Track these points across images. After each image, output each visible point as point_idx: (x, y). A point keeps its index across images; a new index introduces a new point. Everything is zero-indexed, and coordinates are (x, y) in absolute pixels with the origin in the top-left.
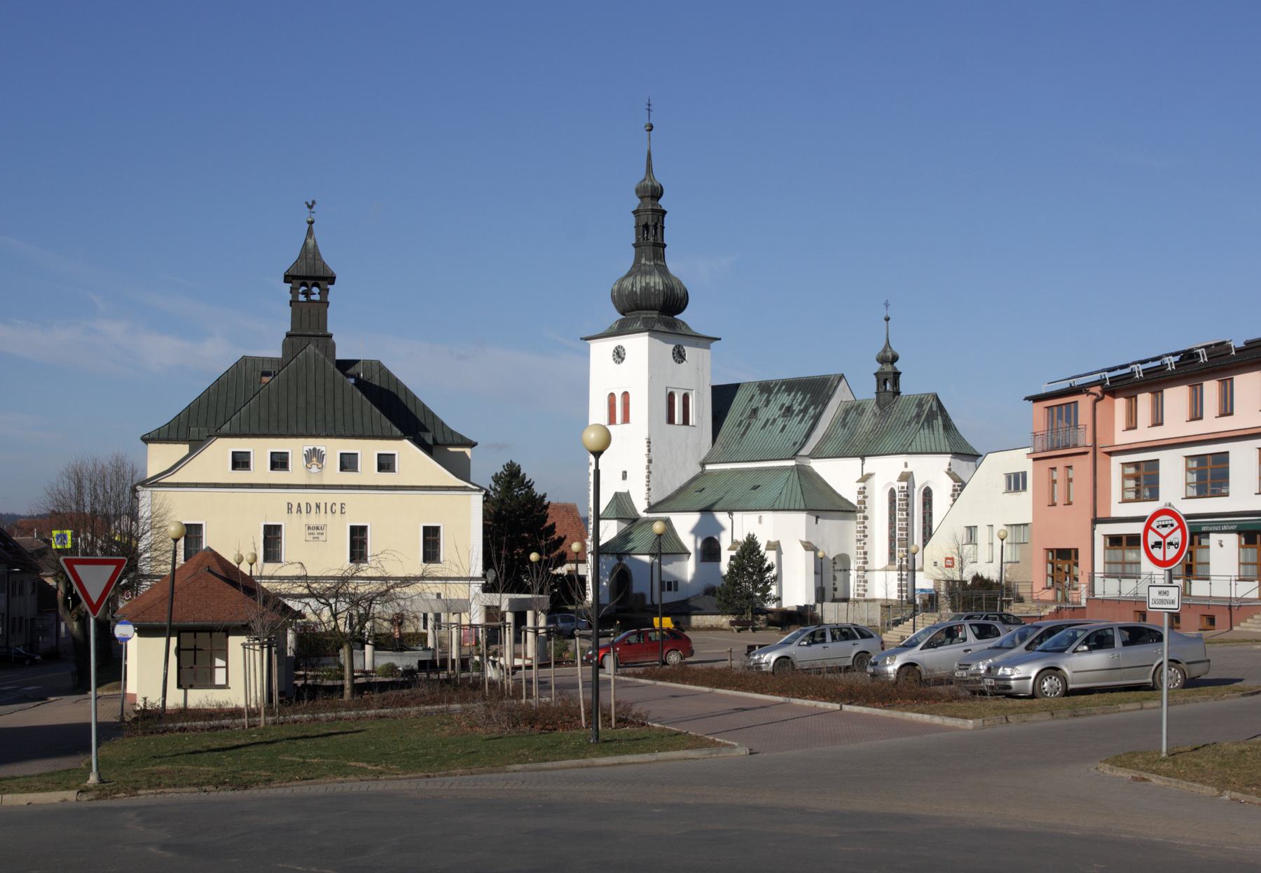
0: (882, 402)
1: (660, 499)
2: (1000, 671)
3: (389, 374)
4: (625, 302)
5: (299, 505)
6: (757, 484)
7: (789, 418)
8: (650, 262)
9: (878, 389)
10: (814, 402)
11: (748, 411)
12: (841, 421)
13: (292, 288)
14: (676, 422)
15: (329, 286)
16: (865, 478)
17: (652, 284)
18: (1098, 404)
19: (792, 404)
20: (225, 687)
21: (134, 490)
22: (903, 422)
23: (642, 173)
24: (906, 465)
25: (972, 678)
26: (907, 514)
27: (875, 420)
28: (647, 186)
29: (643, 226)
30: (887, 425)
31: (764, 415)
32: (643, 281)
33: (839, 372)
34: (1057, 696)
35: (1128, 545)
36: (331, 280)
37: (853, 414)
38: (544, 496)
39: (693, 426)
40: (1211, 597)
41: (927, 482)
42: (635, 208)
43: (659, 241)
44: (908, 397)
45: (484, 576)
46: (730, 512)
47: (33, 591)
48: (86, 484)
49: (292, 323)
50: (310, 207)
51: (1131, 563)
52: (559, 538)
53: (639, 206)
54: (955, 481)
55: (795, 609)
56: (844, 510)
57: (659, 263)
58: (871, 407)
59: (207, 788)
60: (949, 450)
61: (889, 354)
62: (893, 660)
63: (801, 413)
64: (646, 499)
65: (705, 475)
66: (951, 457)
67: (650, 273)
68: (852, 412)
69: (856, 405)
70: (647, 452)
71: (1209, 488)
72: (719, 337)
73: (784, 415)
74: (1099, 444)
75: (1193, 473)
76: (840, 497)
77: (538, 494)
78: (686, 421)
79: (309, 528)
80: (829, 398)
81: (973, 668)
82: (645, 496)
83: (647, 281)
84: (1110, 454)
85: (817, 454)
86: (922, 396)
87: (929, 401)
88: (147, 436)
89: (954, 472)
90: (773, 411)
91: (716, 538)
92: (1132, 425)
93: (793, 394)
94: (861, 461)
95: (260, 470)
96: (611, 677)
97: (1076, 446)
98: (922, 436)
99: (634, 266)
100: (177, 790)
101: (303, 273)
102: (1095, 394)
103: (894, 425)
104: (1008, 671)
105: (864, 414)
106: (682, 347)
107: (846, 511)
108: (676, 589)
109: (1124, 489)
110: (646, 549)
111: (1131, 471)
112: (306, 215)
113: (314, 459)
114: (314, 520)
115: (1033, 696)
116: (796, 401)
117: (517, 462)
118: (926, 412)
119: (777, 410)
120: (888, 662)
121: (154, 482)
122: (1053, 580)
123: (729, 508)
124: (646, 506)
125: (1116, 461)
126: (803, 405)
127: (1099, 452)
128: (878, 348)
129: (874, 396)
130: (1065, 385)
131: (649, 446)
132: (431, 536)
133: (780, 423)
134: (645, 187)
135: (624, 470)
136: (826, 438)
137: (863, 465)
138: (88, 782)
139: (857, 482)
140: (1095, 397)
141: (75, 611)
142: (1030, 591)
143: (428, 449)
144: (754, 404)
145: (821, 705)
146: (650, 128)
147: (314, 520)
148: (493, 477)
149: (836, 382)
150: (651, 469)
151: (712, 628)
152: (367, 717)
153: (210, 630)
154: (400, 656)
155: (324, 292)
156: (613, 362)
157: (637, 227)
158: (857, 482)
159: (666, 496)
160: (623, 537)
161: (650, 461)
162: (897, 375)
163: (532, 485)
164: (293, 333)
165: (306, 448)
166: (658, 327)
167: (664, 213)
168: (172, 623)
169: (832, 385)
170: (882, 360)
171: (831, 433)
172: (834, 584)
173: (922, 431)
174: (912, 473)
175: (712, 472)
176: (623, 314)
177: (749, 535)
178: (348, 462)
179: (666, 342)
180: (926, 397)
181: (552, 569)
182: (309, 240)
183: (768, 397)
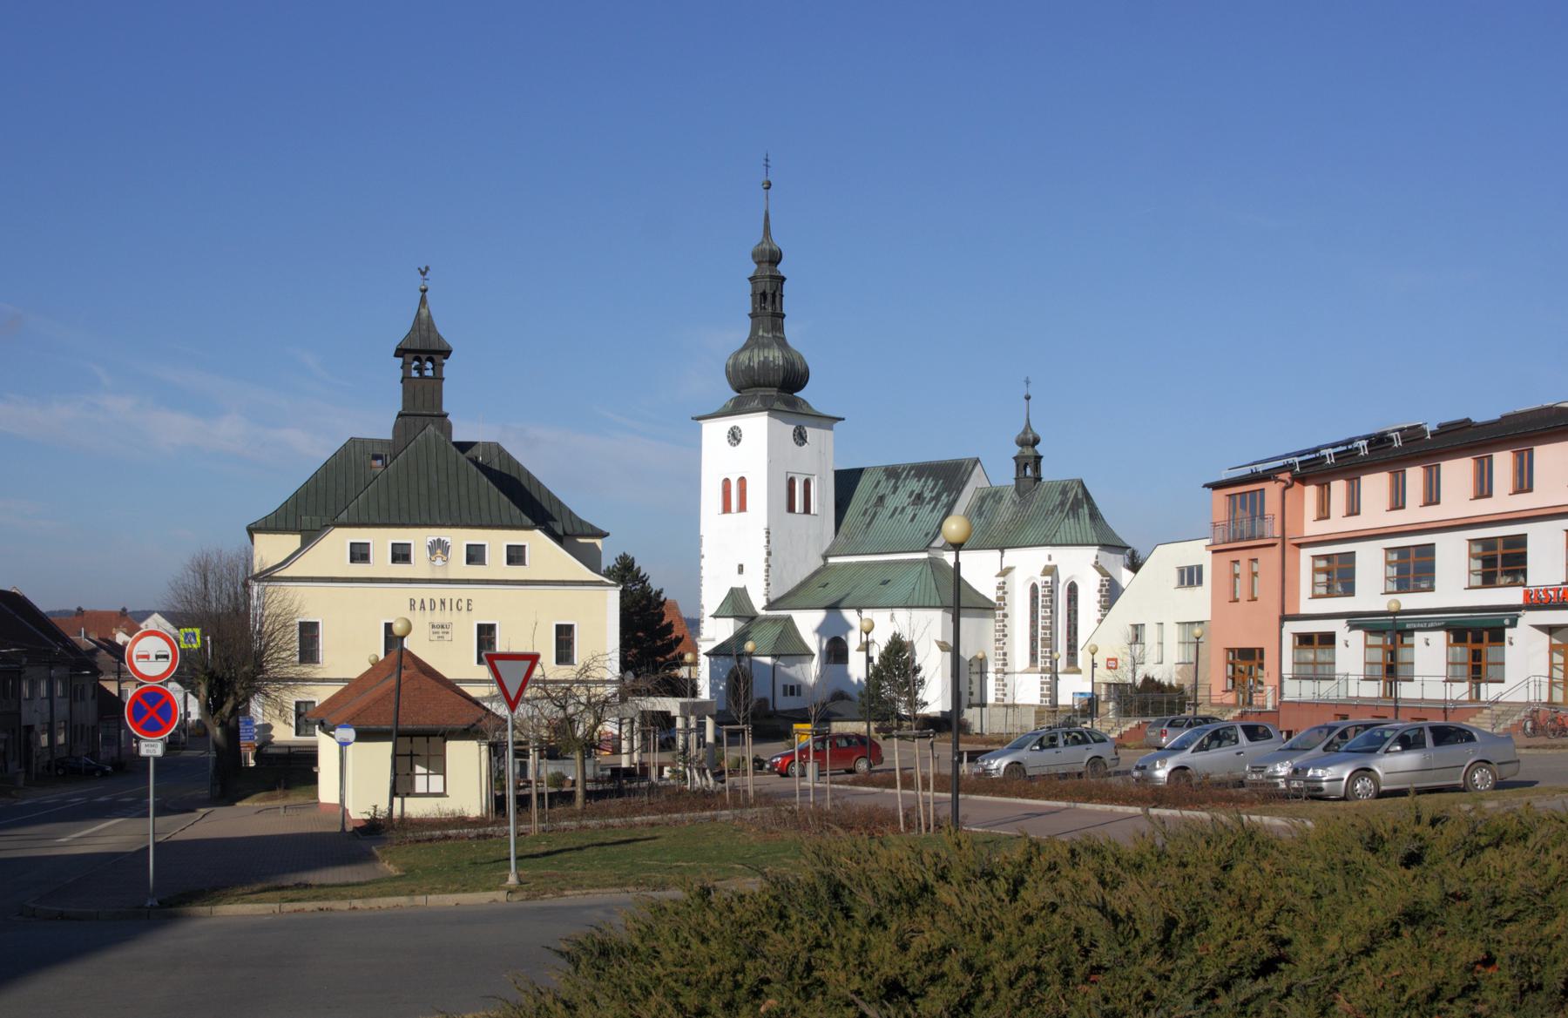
0: (1022, 488)
1: (780, 595)
2: (1310, 773)
3: (509, 457)
5: (422, 601)
6: (887, 578)
9: (1017, 474)
11: (874, 499)
13: (404, 363)
14: (797, 510)
15: (444, 361)
16: (1005, 572)
17: (771, 359)
18: (1287, 492)
19: (922, 492)
20: (443, 795)
21: (246, 585)
23: (758, 236)
24: (1050, 558)
25: (1269, 781)
26: (1051, 612)
31: (892, 502)
32: (761, 354)
33: (972, 455)
34: (1488, 789)
35: (1320, 644)
36: (446, 353)
37: (989, 503)
38: (661, 592)
40: (1423, 699)
41: (1072, 577)
42: (751, 275)
43: (778, 311)
45: (622, 679)
46: (859, 610)
47: (93, 697)
48: (211, 577)
49: (404, 401)
50: (423, 273)
51: (1324, 663)
52: (677, 637)
53: (756, 272)
54: (1103, 575)
55: (939, 715)
56: (985, 608)
57: (778, 334)
58: (1010, 495)
59: (629, 889)
60: (1096, 541)
61: (1030, 436)
62: (1163, 764)
67: (768, 346)
70: (765, 544)
71: (1412, 582)
73: (914, 503)
74: (1288, 534)
75: (1393, 567)
76: (976, 592)
78: (807, 510)
79: (433, 626)
80: (964, 484)
81: (1270, 770)
84: (1299, 546)
88: (253, 526)
90: (901, 498)
91: (843, 637)
92: (1324, 514)
93: (923, 480)
94: (1000, 553)
95: (381, 563)
96: (811, 785)
97: (1262, 537)
98: (1067, 526)
99: (750, 338)
100: (601, 891)
101: (417, 346)
102: (1283, 481)
104: (1320, 772)
108: (799, 694)
109: (1314, 584)
110: (768, 651)
111: (1322, 564)
112: (418, 282)
113: (439, 551)
114: (439, 617)
115: (1345, 799)
116: (928, 487)
117: (631, 554)
120: (1158, 766)
121: (267, 576)
122: (1234, 682)
123: (857, 605)
124: (764, 603)
125: (1306, 554)
127: (1289, 544)
128: (1018, 430)
129: (1013, 482)
130: (1246, 471)
131: (768, 537)
132: (564, 635)
134: (763, 251)
138: (509, 883)
140: (1284, 485)
141: (217, 715)
142: (1207, 693)
143: (558, 539)
144: (881, 491)
145: (1120, 809)
146: (768, 186)
147: (439, 617)
150: (770, 562)
152: (636, 825)
153: (428, 734)
154: (563, 764)
155: (438, 368)
156: (728, 445)
157: (754, 294)
159: (786, 591)
160: (741, 637)
161: (769, 554)
162: (1038, 458)
164: (406, 412)
165: (430, 539)
166: (778, 405)
167: (783, 279)
168: (400, 727)
169: (966, 469)
170: (1022, 443)
173: (1066, 520)
175: (835, 565)
176: (739, 392)
177: (895, 634)
178: (475, 555)
179: (787, 423)
182: (422, 310)
183: (896, 483)
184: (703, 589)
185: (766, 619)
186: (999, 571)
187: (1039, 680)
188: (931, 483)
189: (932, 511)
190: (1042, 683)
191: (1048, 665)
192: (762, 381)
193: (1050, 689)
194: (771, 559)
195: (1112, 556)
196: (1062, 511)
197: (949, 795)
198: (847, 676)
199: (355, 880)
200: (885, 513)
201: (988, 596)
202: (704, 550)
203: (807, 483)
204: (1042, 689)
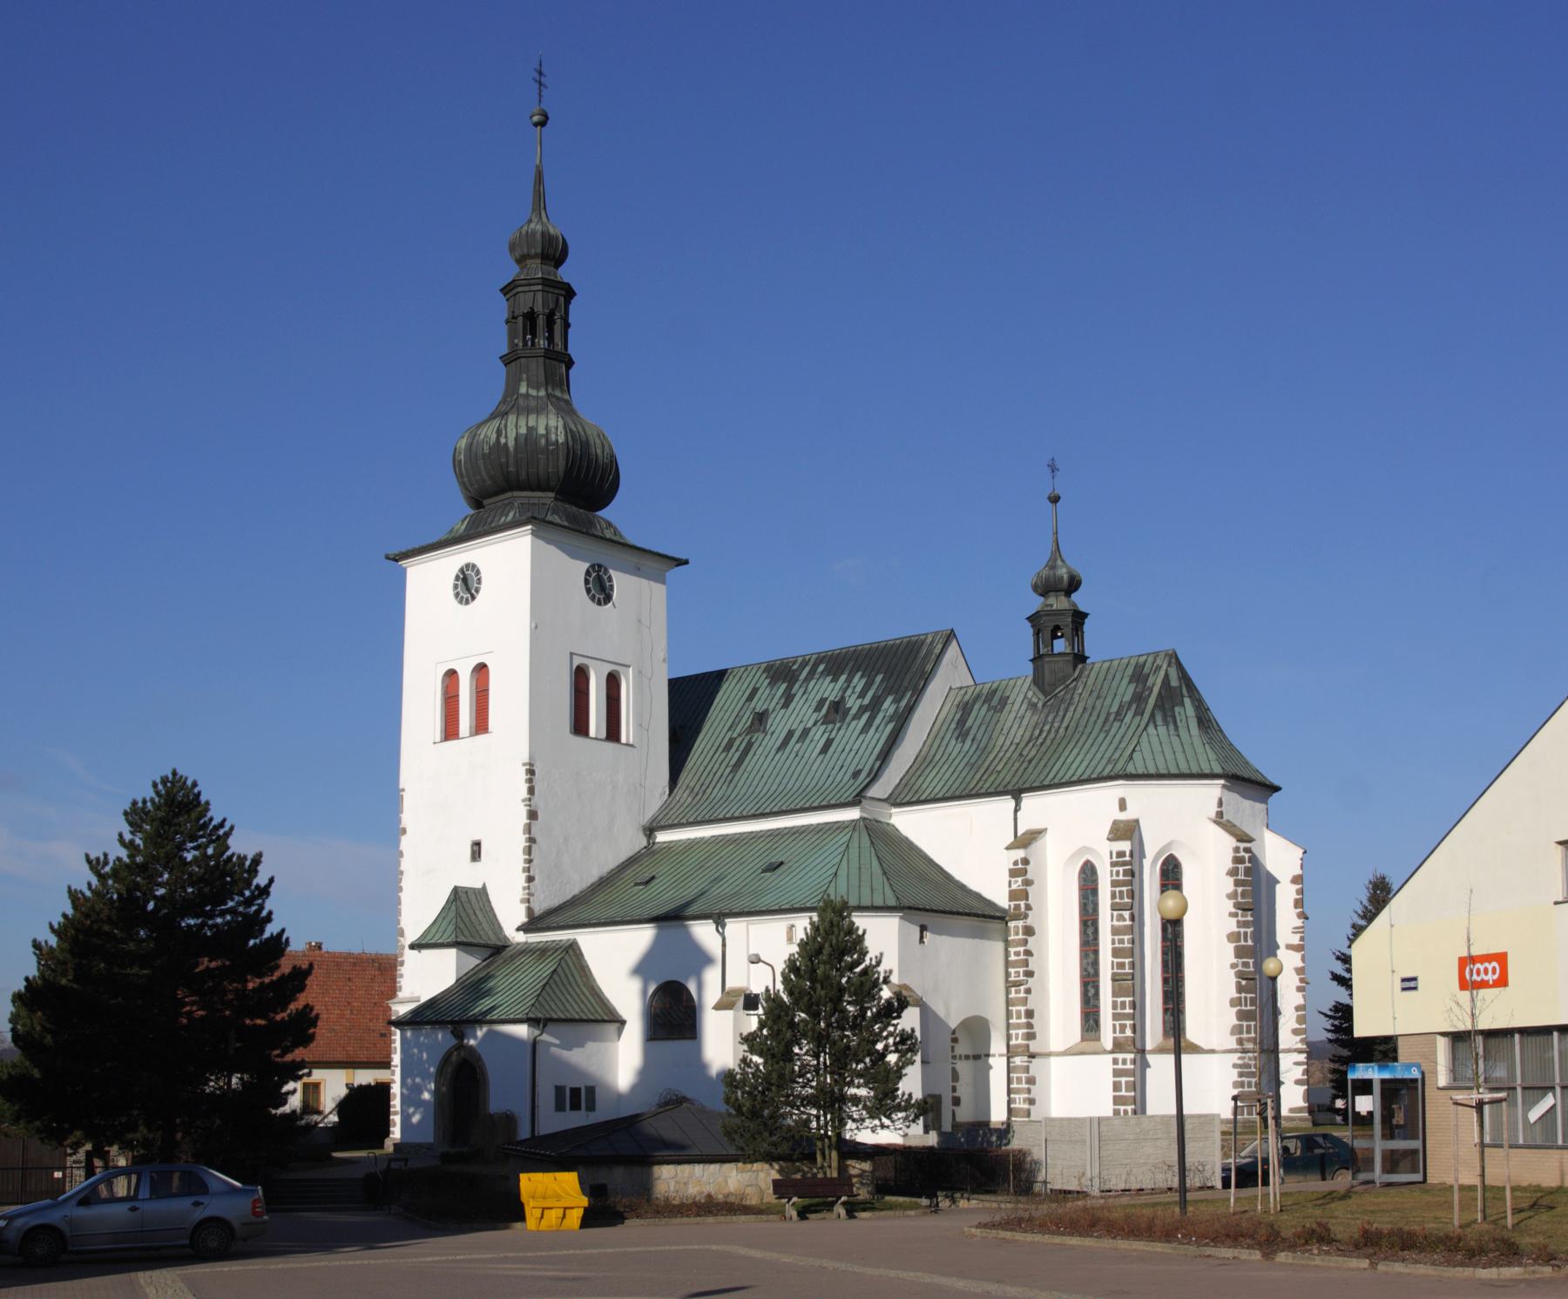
1: (556, 902)
4: (484, 473)
6: (776, 859)
7: (838, 725)
8: (538, 390)
10: (894, 687)
12: (953, 726)
14: (592, 732)
16: (1026, 840)
17: (542, 431)
19: (843, 697)
24: (1123, 805)
26: (1132, 918)
27: (1035, 718)
28: (534, 233)
29: (525, 316)
30: (1064, 725)
31: (779, 723)
32: (522, 422)
33: (945, 626)
37: (979, 712)
39: (627, 745)
41: (1169, 845)
43: (559, 347)
44: (1107, 664)
46: (719, 919)
53: (518, 275)
57: (558, 393)
60: (1217, 769)
61: (1062, 572)
64: (522, 901)
65: (654, 853)
66: (1224, 786)
67: (539, 410)
68: (977, 707)
69: (985, 692)
70: (524, 794)
72: (683, 557)
73: (827, 720)
76: (963, 887)
78: (613, 733)
80: (927, 678)
82: (520, 894)
83: (530, 424)
85: (905, 797)
86: (1142, 660)
87: (1159, 668)
89: (1228, 821)
90: (803, 712)
93: (843, 678)
98: (1155, 740)
103: (1083, 723)
105: (1007, 708)
106: (606, 571)
107: (984, 916)
110: (521, 1010)
117: (189, 773)
118: (1156, 690)
119: (810, 711)
126: (870, 694)
128: (1035, 565)
131: (530, 781)
133: (819, 736)
134: (530, 236)
135: (476, 838)
136: (923, 763)
137: (1016, 811)
139: (1008, 848)
144: (759, 704)
148: (126, 813)
149: (940, 646)
150: (536, 832)
151: (709, 1207)
157: (512, 319)
158: (1008, 848)
159: (568, 897)
160: (470, 988)
161: (533, 815)
162: (1079, 617)
163: (228, 834)
169: (929, 652)
170: (1045, 588)
172: (954, 1089)
173: (1151, 729)
174: (1137, 821)
175: (670, 846)
180: (1151, 659)
181: (277, 1052)
183: (789, 688)
184: (405, 896)
185: (527, 950)
186: (1012, 839)
187: (1110, 1067)
188: (859, 682)
190: (1117, 1073)
191: (1129, 1033)
192: (523, 476)
193: (1132, 1086)
194: (536, 826)
195: (1247, 803)
197: (397, 1035)
198: (701, 1066)
200: (767, 743)
201: (988, 894)
202: (407, 819)
203: (613, 682)
204: (1117, 1087)
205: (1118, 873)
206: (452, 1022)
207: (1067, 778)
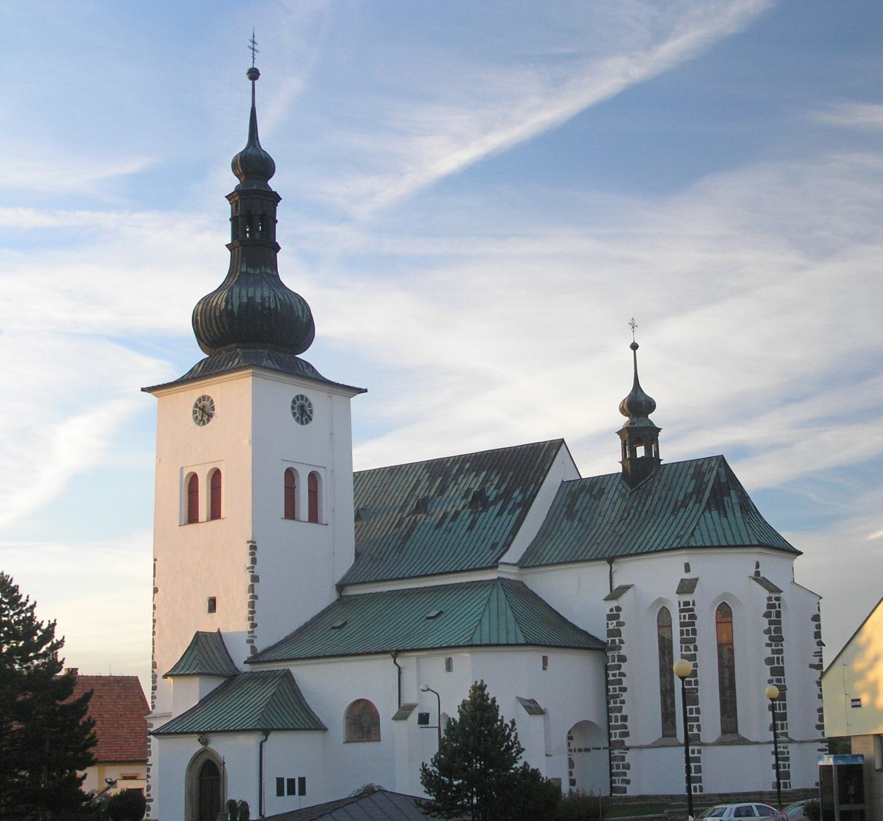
12: (565, 509)
17: (258, 300)
19: (484, 489)
22: (673, 504)
24: (687, 568)
27: (624, 504)
30: (645, 509)
32: (244, 293)
63: (500, 499)
70: (249, 565)
77: (66, 666)
81: (10, 724)
105: (604, 496)
108: (302, 792)
119: (460, 498)
124: (248, 654)
131: (252, 554)
136: (544, 534)
146: (254, 74)
161: (255, 579)
171: (550, 529)
173: (707, 514)
185: (252, 677)
186: (608, 592)
189: (500, 513)
194: (257, 568)
196: (699, 501)
199: (734, 532)
205: (685, 616)
206: (199, 733)
207: (647, 549)
